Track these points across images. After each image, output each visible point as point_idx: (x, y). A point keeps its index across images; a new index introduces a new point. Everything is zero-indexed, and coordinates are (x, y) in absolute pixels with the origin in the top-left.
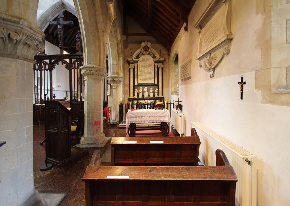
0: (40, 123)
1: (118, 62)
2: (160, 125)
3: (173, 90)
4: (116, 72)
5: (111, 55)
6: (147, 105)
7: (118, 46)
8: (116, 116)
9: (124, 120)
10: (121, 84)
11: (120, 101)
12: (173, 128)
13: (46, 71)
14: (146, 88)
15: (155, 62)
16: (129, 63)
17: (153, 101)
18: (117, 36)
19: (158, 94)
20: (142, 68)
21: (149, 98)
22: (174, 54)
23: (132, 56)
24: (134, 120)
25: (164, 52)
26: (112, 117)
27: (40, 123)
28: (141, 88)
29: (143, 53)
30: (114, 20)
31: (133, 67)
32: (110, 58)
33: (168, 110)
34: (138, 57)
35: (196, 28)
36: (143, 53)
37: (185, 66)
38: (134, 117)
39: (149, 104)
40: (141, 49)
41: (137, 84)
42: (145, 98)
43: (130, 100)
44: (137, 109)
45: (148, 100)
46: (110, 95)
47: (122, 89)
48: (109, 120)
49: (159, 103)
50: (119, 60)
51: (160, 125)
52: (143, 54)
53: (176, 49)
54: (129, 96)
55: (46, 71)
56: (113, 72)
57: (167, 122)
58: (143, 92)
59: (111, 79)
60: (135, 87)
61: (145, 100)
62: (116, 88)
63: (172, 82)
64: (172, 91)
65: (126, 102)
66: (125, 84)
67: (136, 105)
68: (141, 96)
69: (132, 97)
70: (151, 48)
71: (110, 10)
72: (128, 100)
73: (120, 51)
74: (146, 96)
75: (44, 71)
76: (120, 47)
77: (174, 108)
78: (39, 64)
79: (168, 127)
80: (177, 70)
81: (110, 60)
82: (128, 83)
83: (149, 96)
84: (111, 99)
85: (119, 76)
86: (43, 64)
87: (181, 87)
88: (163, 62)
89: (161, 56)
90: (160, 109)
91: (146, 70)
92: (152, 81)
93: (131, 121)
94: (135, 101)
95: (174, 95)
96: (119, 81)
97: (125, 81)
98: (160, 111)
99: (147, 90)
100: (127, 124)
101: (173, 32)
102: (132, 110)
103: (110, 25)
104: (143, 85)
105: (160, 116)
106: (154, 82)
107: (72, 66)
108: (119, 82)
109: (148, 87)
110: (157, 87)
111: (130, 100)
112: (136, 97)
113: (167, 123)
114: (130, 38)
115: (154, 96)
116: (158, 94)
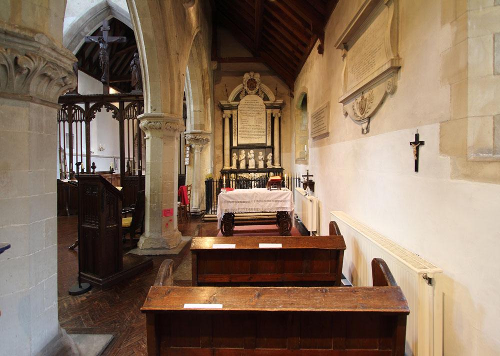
0: (68, 213)
1: (203, 108)
2: (276, 217)
3: (298, 156)
4: (201, 124)
5: (191, 94)
6: (253, 182)
7: (203, 80)
8: (199, 200)
9: (213, 207)
10: (208, 145)
11: (208, 175)
12: (299, 222)
13: (79, 123)
14: (252, 151)
15: (267, 107)
16: (222, 109)
17: (264, 174)
18: (201, 62)
19: (273, 163)
20: (244, 117)
21: (256, 170)
22: (300, 94)
23: (228, 96)
24: (231, 208)
25: (283, 89)
26: (193, 202)
27: (68, 213)
28: (243, 152)
29: (246, 92)
30: (197, 35)
31: (230, 116)
32: (189, 100)
33: (289, 191)
34: (237, 99)
35: (337, 49)
36: (246, 92)
37: (320, 114)
38: (231, 202)
39: (257, 180)
40: (244, 85)
41: (236, 145)
42: (250, 169)
43: (223, 172)
44: (237, 188)
45: (255, 172)
46: (190, 165)
47: (211, 153)
48: (188, 208)
49: (274, 179)
50: (205, 104)
51: (276, 217)
52: (246, 94)
53: (303, 85)
54: (222, 165)
55: (79, 123)
56: (194, 125)
57: (289, 210)
58: (247, 159)
59: (191, 137)
60: (233, 150)
61: (249, 172)
62: (199, 152)
63: (297, 142)
64: (297, 157)
65: (217, 177)
66: (216, 145)
67: (234, 182)
68: (242, 166)
69: (227, 167)
70: (260, 83)
71: (190, 18)
72: (221, 173)
73: (207, 88)
74: (252, 166)
75: (77, 123)
76: (207, 81)
77: (299, 187)
78: (66, 111)
79: (290, 220)
80: (305, 122)
81: (190, 104)
82: (221, 143)
83: (257, 165)
84: (192, 171)
85: (206, 132)
86: (74, 111)
87: (312, 151)
88: (280, 107)
89: (277, 96)
90: (277, 188)
91: (252, 121)
92: (261, 140)
93: (226, 210)
94: (233, 175)
95: (300, 164)
96: (206, 140)
97: (216, 140)
98: (276, 192)
99: (253, 155)
100: (219, 215)
101: (298, 55)
102: (227, 191)
103: (190, 43)
104: (247, 147)
105: (276, 201)
106: (265, 142)
107: (125, 114)
108: (205, 142)
109: (256, 150)
110: (271, 150)
111: (223, 172)
112: (234, 167)
113: (287, 213)
114: (224, 66)
115: (265, 165)
116: (273, 163)
